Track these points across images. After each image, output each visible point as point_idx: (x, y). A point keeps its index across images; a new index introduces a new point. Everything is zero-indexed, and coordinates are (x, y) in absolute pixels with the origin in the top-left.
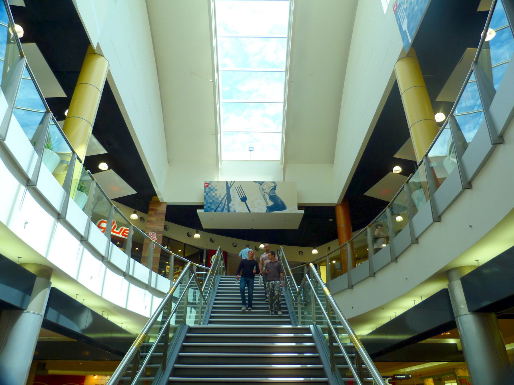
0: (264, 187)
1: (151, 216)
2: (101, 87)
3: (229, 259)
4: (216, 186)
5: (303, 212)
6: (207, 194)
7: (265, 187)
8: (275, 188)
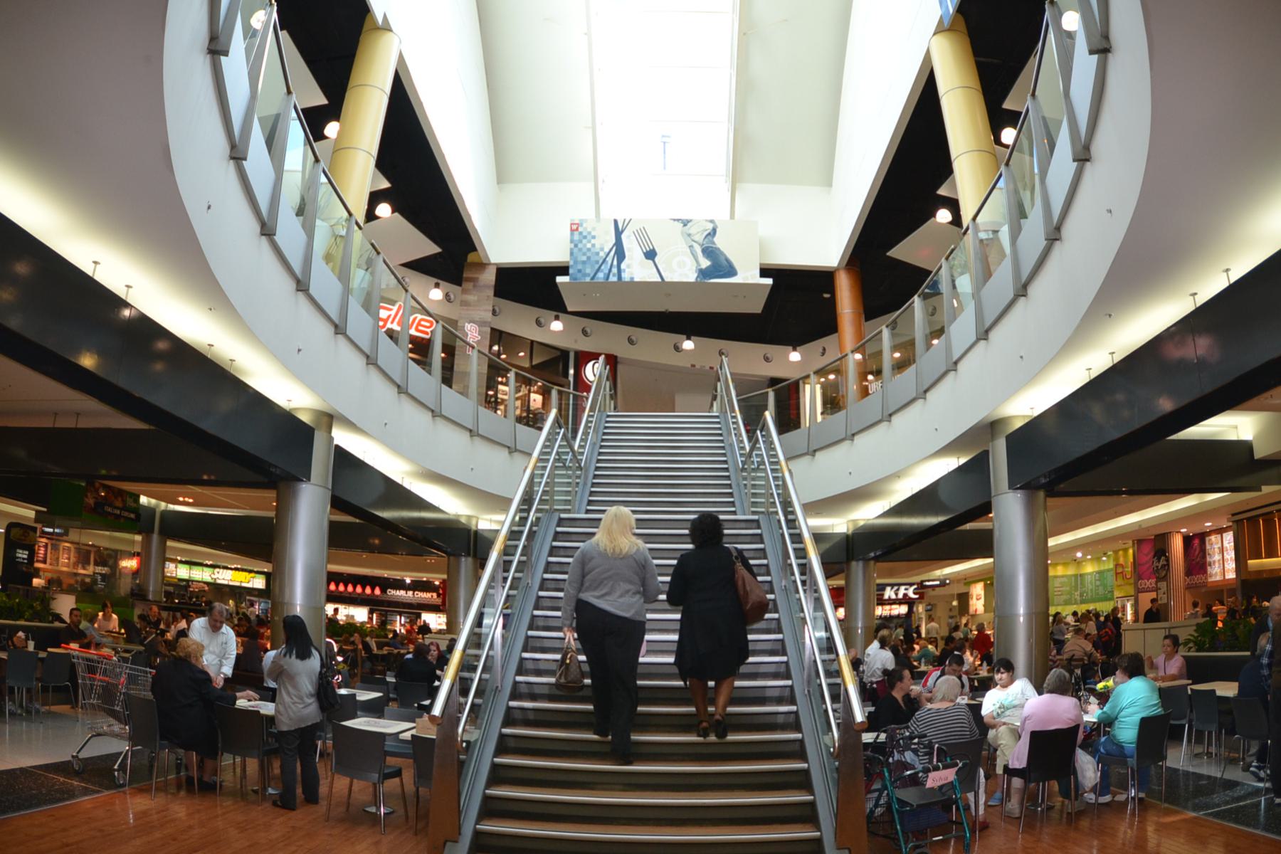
0: (692, 229)
1: (465, 292)
2: (388, 87)
3: (621, 369)
4: (594, 229)
5: (769, 281)
6: (576, 246)
7: (692, 231)
8: (714, 232)
